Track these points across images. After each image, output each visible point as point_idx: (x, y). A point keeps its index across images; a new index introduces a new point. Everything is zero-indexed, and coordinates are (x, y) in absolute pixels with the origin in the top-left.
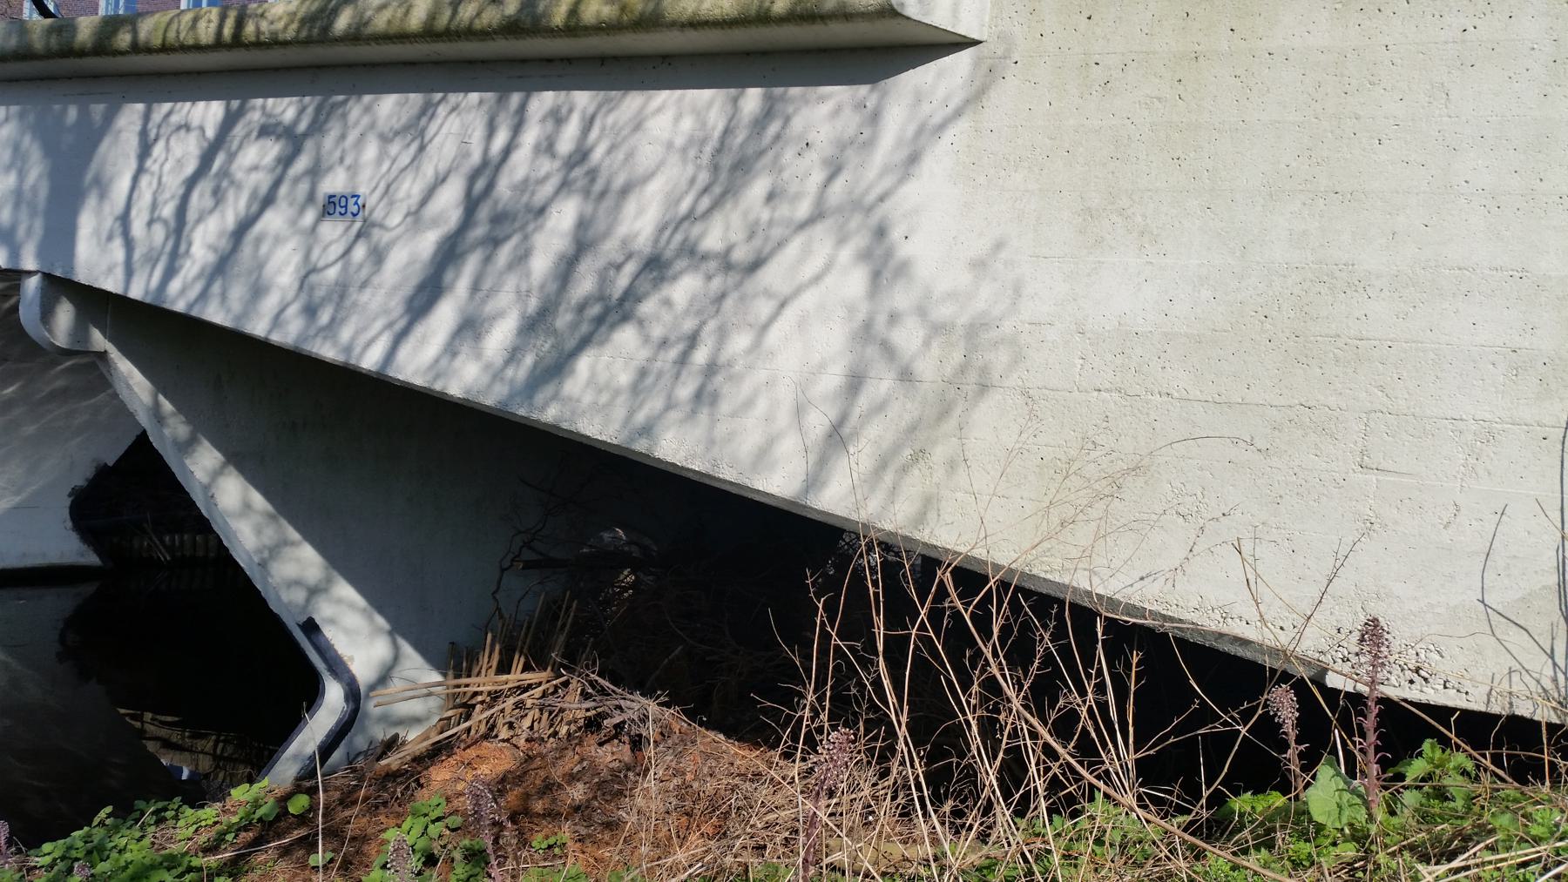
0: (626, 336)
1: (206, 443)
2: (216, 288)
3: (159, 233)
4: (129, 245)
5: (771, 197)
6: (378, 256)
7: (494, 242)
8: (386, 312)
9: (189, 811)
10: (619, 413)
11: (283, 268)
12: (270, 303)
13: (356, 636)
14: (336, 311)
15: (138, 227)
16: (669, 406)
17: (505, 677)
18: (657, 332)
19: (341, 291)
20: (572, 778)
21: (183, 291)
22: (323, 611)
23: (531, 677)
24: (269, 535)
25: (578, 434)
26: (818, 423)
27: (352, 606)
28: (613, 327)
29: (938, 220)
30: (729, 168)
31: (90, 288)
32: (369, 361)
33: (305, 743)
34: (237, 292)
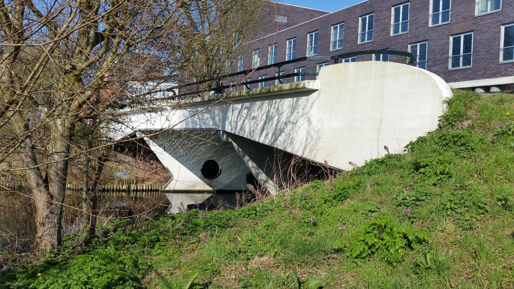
0: (283, 134)
4: (231, 126)
5: (298, 113)
6: (257, 125)
7: (270, 122)
12: (246, 133)
19: (253, 131)
22: (267, 185)
26: (303, 145)
29: (315, 113)
30: (293, 109)
32: (257, 140)
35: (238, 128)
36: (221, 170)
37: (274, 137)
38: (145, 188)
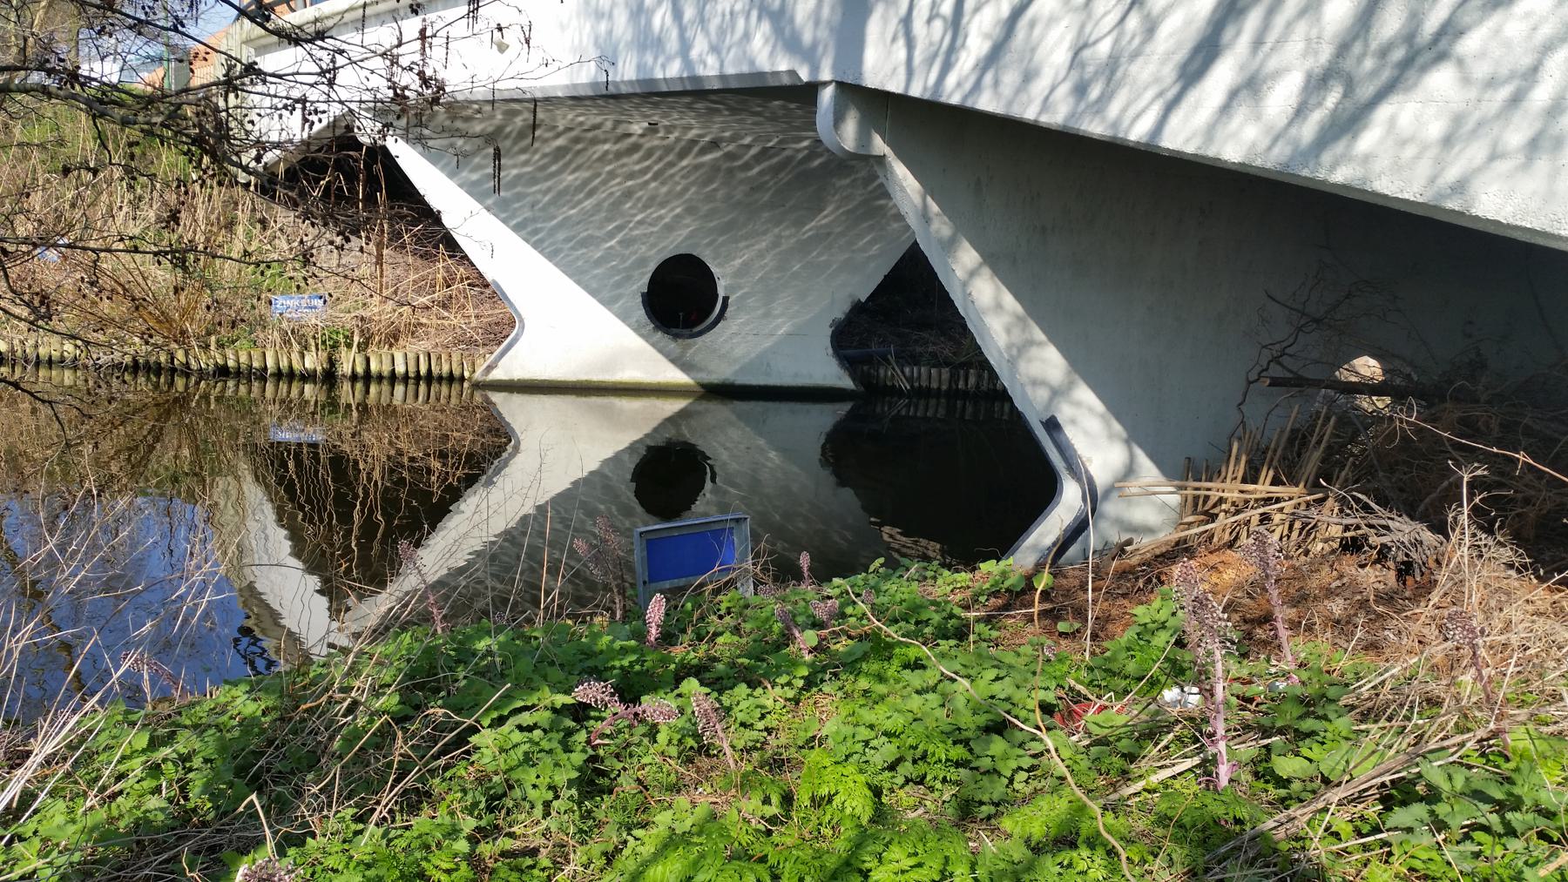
0: (1441, 80)
1: (966, 244)
2: (988, 78)
3: (938, 25)
6: (1150, 29)
8: (1157, 80)
9: (946, 573)
10: (1424, 169)
11: (1055, 52)
12: (1040, 87)
13: (1094, 440)
14: (1108, 85)
15: (919, 26)
16: (1494, 156)
17: (1251, 487)
18: (1481, 70)
20: (1330, 593)
21: (959, 85)
22: (1064, 413)
23: (1278, 490)
24: (1017, 336)
25: (1375, 194)
27: (1091, 410)
28: (1424, 69)
31: (876, 90)
32: (1137, 133)
33: (1042, 535)
34: (1010, 78)
35: (966, 61)
36: (726, 299)
37: (1333, 98)
38: (400, 369)
